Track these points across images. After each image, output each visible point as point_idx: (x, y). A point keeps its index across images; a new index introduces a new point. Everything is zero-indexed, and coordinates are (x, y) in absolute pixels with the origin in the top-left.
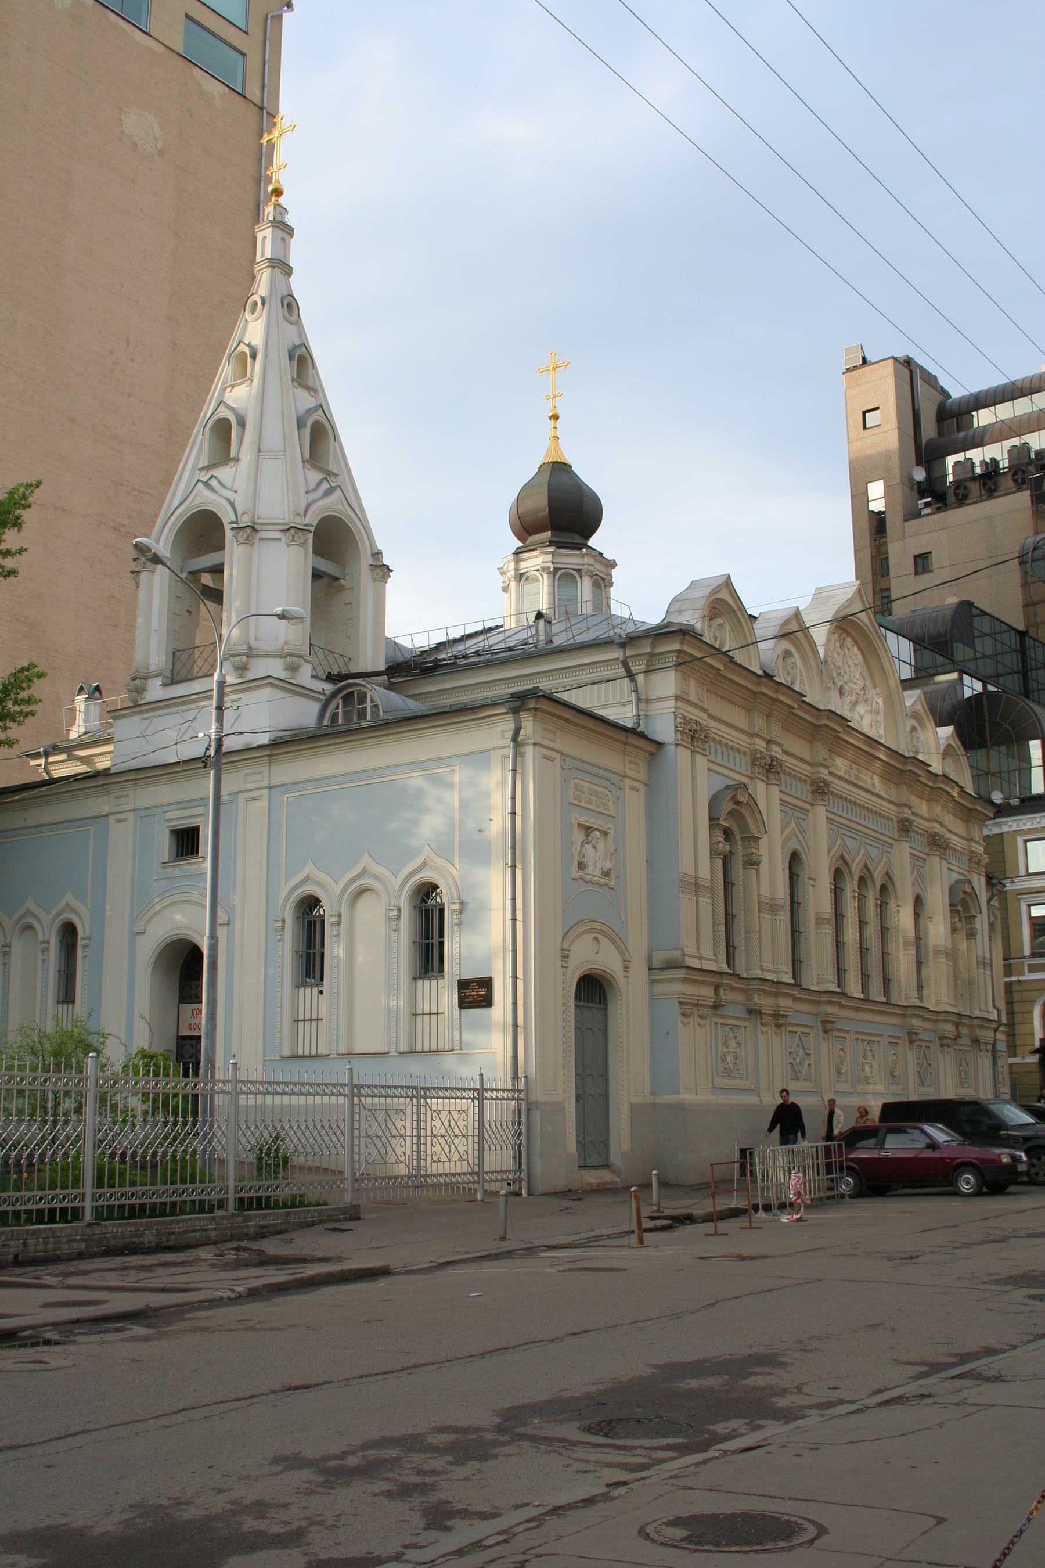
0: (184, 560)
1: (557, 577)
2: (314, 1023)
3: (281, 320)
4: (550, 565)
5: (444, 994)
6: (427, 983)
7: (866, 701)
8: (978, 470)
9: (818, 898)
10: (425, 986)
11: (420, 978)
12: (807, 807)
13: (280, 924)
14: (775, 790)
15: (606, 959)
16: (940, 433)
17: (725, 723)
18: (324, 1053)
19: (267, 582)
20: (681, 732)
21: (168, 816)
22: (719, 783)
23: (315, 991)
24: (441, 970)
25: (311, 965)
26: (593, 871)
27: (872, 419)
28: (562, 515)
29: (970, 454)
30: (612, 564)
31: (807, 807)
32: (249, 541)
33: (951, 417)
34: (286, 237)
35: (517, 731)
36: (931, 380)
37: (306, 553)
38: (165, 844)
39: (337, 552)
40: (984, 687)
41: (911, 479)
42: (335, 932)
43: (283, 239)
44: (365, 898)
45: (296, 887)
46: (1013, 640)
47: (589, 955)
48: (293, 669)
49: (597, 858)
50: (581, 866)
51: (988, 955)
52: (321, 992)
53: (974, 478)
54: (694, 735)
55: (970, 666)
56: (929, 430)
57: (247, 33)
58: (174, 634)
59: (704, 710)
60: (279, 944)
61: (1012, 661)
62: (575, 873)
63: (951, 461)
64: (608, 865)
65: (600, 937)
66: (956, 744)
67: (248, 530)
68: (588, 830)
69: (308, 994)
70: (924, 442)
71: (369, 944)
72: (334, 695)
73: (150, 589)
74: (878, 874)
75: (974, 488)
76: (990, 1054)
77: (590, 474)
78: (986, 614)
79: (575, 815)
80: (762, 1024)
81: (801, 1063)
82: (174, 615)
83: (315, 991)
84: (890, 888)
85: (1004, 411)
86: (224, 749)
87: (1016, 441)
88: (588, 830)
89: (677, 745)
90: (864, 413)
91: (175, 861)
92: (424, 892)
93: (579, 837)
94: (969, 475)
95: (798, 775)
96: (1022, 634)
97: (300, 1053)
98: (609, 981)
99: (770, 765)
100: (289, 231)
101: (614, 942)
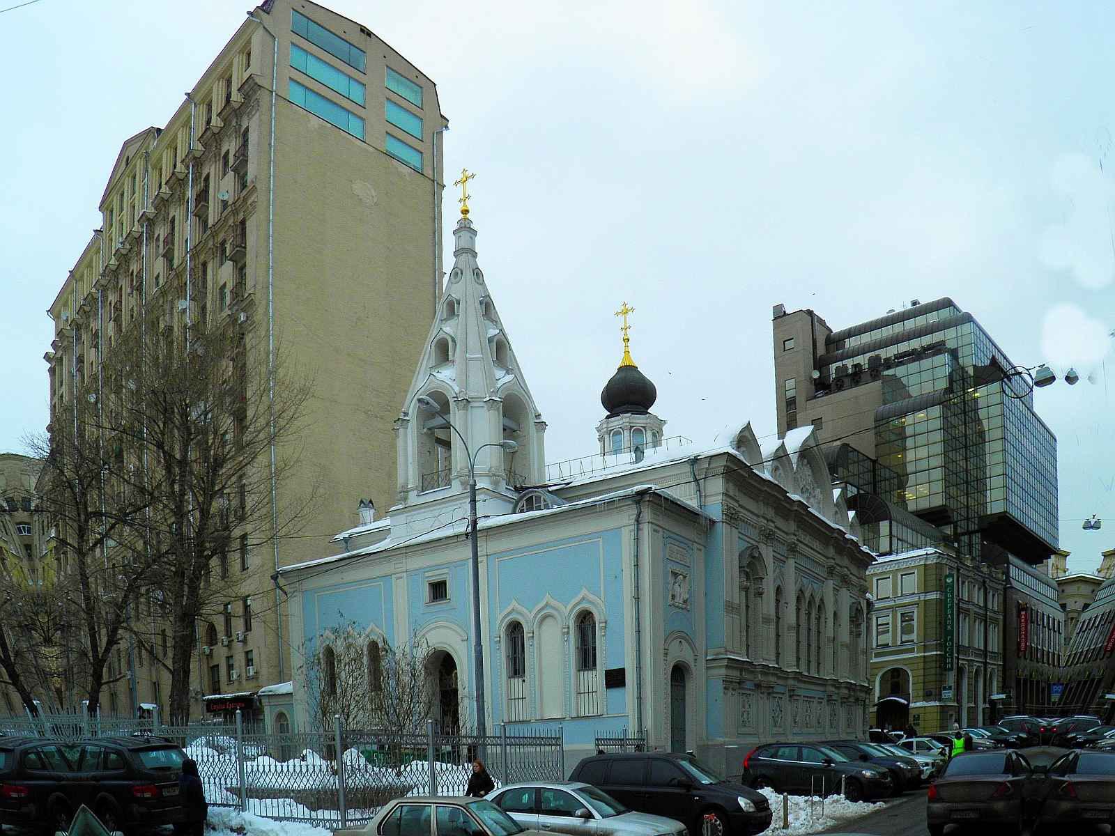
0: (424, 421)
1: (611, 435)
2: (521, 701)
3: (473, 282)
4: (627, 424)
5: (596, 678)
6: (516, 680)
7: (814, 497)
8: (850, 371)
9: (790, 615)
10: (585, 675)
11: (512, 677)
12: (785, 559)
13: (531, 635)
14: (771, 549)
15: (686, 655)
16: (827, 350)
17: (747, 510)
18: (528, 719)
19: (478, 432)
20: (725, 514)
21: (427, 574)
22: (744, 545)
23: (520, 680)
24: (594, 664)
25: (517, 668)
26: (679, 600)
27: (789, 345)
28: (629, 395)
29: (844, 362)
30: (663, 422)
31: (785, 559)
32: (465, 408)
33: (834, 343)
34: (472, 236)
35: (639, 516)
36: (822, 322)
37: (499, 414)
38: (426, 593)
39: (515, 414)
40: (858, 492)
41: (811, 377)
42: (603, 634)
43: (471, 238)
44: (548, 622)
45: (574, 607)
46: (868, 464)
47: (681, 653)
48: (496, 483)
49: (682, 592)
50: (673, 597)
51: (865, 647)
52: (524, 681)
53: (847, 375)
54: (732, 517)
55: (851, 480)
56: (821, 350)
57: (422, 141)
58: (421, 465)
59: (737, 501)
60: (498, 652)
61: (868, 477)
62: (670, 601)
63: (833, 367)
64: (687, 596)
65: (682, 641)
66: (857, 523)
67: (465, 402)
68: (675, 575)
69: (516, 682)
70: (818, 356)
71: (551, 649)
72: (521, 499)
73: (406, 435)
74: (817, 599)
75: (847, 381)
76: (862, 708)
77: (648, 371)
78: (856, 450)
79: (669, 565)
80: (761, 693)
81: (778, 716)
82: (420, 453)
83: (520, 680)
84: (822, 606)
85: (866, 338)
86: (478, 527)
87: (872, 354)
88: (675, 575)
89: (723, 522)
90: (784, 342)
91: (433, 602)
92: (582, 616)
93: (671, 579)
94: (845, 374)
95: (781, 541)
96: (874, 462)
97: (513, 720)
98: (684, 667)
99: (769, 534)
100: (475, 233)
101: (689, 644)
